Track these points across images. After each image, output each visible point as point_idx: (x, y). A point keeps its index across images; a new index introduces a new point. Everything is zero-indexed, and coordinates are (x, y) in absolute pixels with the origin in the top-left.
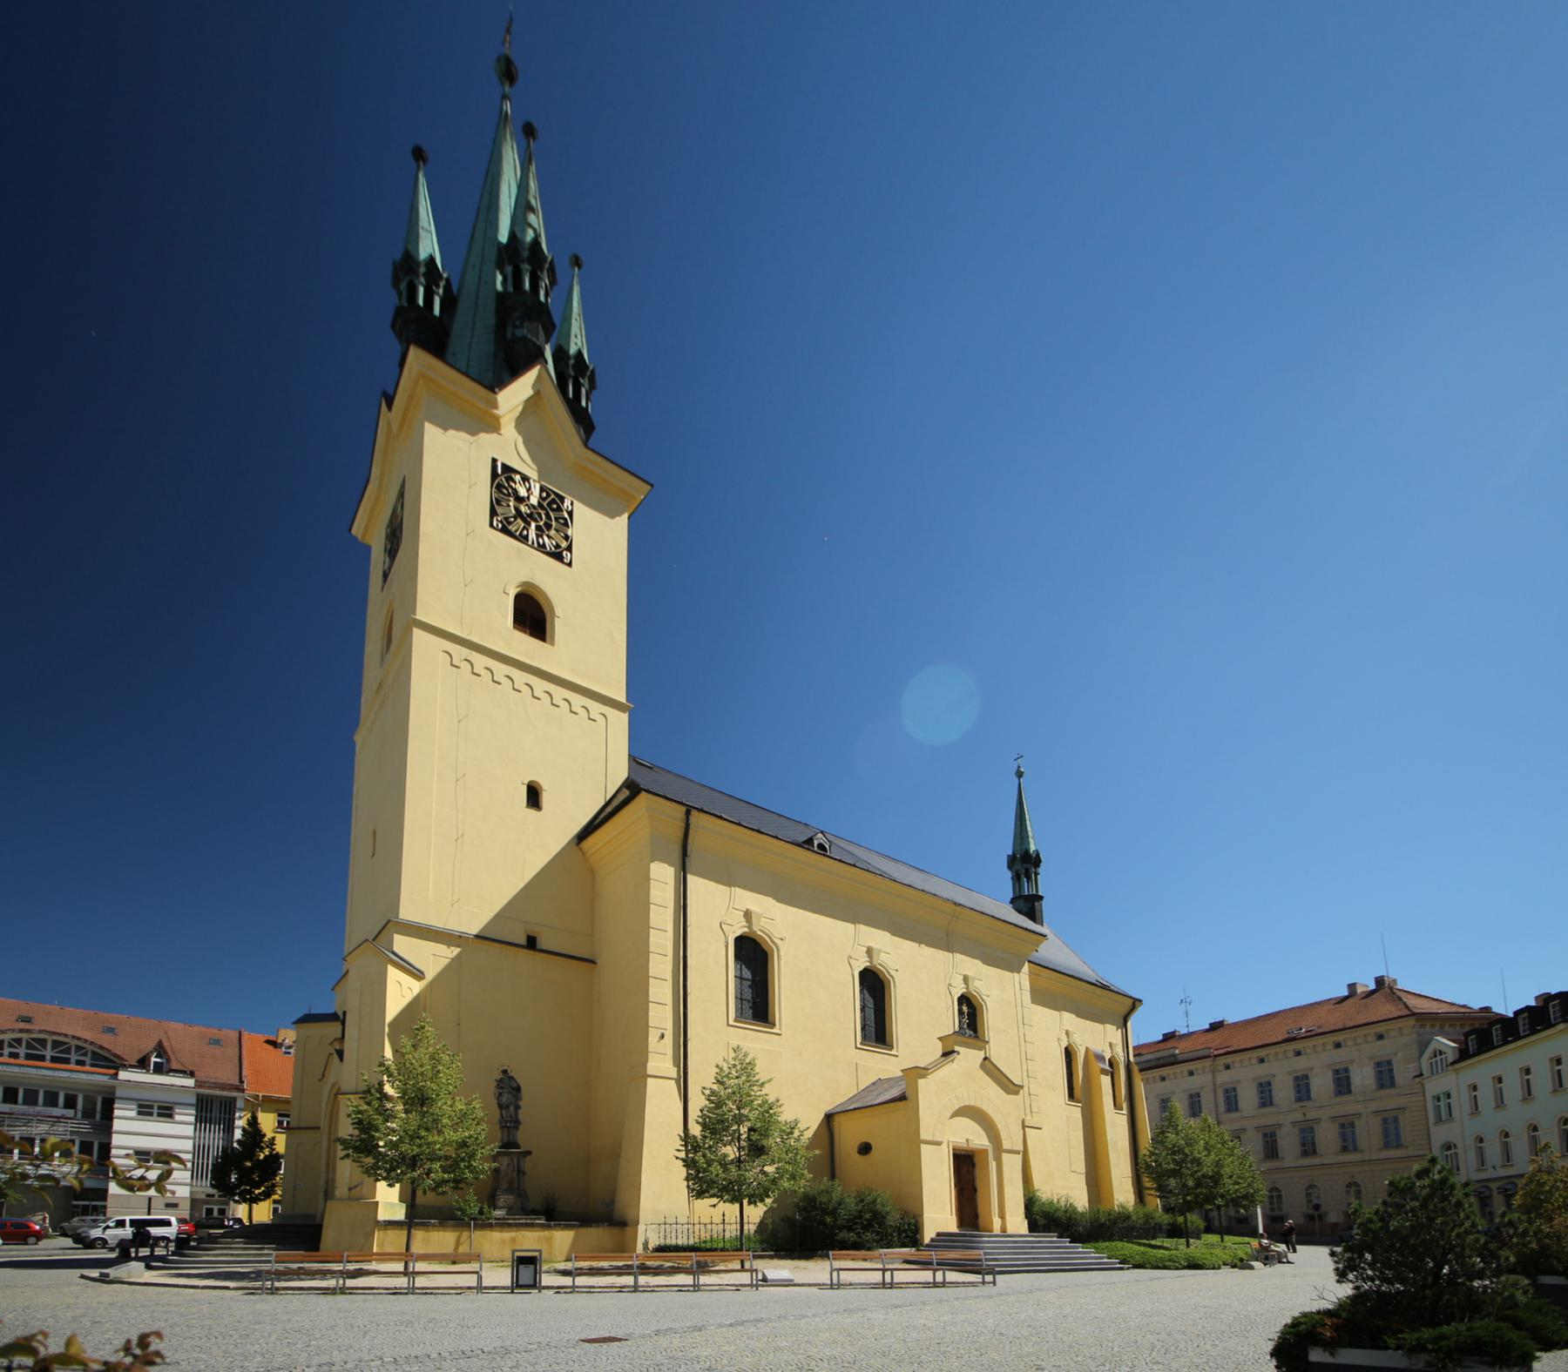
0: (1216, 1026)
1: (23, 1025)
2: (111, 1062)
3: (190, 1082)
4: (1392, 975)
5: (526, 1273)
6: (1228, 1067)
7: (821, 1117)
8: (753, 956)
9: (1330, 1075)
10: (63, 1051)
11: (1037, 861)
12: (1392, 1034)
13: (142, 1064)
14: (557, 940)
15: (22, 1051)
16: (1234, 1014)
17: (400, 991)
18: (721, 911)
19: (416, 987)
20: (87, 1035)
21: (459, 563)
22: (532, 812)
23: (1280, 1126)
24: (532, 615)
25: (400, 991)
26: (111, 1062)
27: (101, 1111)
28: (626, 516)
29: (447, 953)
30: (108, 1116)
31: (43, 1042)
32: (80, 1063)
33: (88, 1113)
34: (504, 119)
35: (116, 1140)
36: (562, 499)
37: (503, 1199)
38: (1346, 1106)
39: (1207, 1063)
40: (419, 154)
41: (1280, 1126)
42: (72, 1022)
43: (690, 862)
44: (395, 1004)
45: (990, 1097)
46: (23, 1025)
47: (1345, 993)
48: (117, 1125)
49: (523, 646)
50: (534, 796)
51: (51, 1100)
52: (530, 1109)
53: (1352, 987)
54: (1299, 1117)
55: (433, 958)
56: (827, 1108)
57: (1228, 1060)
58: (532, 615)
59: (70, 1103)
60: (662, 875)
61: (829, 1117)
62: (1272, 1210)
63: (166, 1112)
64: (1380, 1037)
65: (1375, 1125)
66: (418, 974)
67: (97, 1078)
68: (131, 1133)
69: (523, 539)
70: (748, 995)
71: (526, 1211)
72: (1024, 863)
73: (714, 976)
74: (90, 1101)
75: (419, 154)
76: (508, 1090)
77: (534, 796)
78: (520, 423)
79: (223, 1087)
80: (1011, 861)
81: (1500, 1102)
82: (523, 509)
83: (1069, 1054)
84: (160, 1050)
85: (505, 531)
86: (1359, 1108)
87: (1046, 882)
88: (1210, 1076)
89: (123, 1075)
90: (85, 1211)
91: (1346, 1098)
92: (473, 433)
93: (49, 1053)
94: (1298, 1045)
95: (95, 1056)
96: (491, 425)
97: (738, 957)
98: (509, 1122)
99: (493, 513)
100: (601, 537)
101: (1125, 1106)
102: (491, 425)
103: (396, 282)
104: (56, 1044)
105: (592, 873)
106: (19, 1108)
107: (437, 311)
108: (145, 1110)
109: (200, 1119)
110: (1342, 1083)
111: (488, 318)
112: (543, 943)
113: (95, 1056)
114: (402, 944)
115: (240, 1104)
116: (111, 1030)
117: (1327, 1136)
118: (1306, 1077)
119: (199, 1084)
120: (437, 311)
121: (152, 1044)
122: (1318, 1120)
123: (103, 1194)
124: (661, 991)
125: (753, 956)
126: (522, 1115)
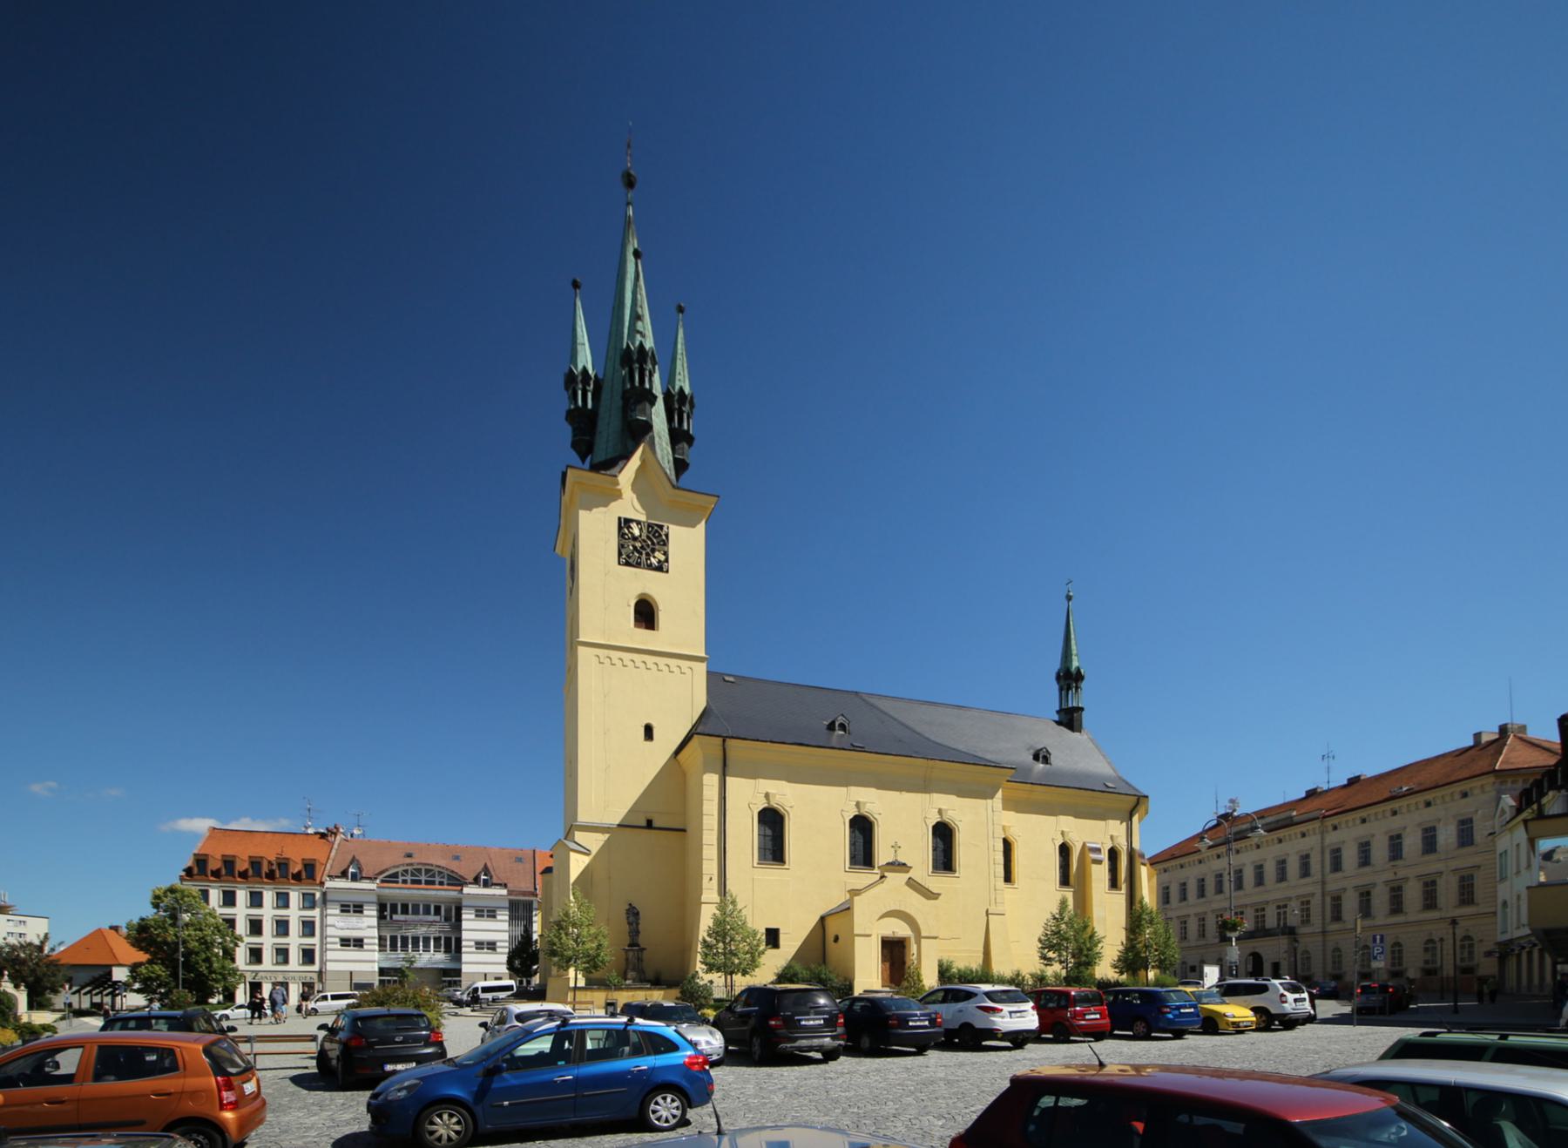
0: (1353, 781)
1: (408, 860)
2: (457, 881)
3: (504, 892)
4: (1518, 720)
5: (611, 1009)
6: (1335, 828)
7: (815, 919)
8: (772, 821)
9: (1419, 834)
11: (1079, 677)
12: (1476, 791)
13: (476, 881)
14: (661, 823)
15: (409, 878)
16: (1369, 770)
17: (577, 864)
18: (747, 796)
19: (586, 860)
20: (443, 863)
21: (604, 588)
22: (648, 743)
23: (1374, 885)
24: (646, 614)
25: (577, 864)
26: (457, 881)
27: (453, 915)
28: (701, 527)
29: (601, 838)
30: (459, 919)
31: (419, 871)
32: (441, 883)
33: (448, 950)
34: (628, 222)
35: (465, 935)
36: (661, 527)
37: (631, 974)
38: (1432, 865)
39: (1316, 824)
40: (576, 285)
41: (1374, 885)
43: (730, 768)
44: (574, 874)
45: (914, 904)
46: (408, 860)
47: (1471, 743)
48: (465, 925)
49: (643, 638)
50: (649, 732)
51: (427, 912)
52: (643, 925)
53: (1477, 736)
54: (1390, 876)
55: (595, 842)
56: (822, 913)
57: (1335, 820)
58: (646, 614)
59: (437, 911)
60: (711, 781)
61: (823, 919)
62: (1393, 964)
63: (492, 914)
64: (1465, 795)
65: (1454, 882)
66: (587, 852)
67: (449, 893)
68: (473, 930)
69: (638, 565)
70: (769, 845)
71: (641, 981)
72: (1069, 679)
73: (745, 835)
74: (448, 911)
75: (576, 285)
76: (633, 914)
77: (649, 732)
78: (635, 486)
79: (524, 894)
80: (1058, 678)
81: (1184, 898)
82: (638, 545)
83: (1065, 850)
84: (486, 870)
85: (628, 564)
86: (1440, 866)
87: (1085, 697)
88: (1319, 837)
89: (466, 890)
90: (450, 984)
91: (1432, 857)
92: (606, 505)
93: (423, 878)
94: (1395, 805)
96: (617, 495)
97: (760, 821)
98: (635, 932)
99: (620, 554)
100: (687, 544)
101: (1124, 886)
102: (617, 495)
103: (567, 389)
104: (427, 871)
105: (684, 774)
106: (410, 917)
107: (590, 405)
108: (480, 913)
109: (512, 918)
110: (1430, 842)
111: (618, 402)
112: (655, 824)
114: (579, 836)
115: (535, 905)
116: (457, 858)
117: (1413, 894)
118: (1399, 836)
119: (510, 893)
120: (590, 405)
121: (481, 866)
122: (1406, 879)
123: (458, 972)
124: (710, 853)
125: (772, 821)
126: (641, 927)
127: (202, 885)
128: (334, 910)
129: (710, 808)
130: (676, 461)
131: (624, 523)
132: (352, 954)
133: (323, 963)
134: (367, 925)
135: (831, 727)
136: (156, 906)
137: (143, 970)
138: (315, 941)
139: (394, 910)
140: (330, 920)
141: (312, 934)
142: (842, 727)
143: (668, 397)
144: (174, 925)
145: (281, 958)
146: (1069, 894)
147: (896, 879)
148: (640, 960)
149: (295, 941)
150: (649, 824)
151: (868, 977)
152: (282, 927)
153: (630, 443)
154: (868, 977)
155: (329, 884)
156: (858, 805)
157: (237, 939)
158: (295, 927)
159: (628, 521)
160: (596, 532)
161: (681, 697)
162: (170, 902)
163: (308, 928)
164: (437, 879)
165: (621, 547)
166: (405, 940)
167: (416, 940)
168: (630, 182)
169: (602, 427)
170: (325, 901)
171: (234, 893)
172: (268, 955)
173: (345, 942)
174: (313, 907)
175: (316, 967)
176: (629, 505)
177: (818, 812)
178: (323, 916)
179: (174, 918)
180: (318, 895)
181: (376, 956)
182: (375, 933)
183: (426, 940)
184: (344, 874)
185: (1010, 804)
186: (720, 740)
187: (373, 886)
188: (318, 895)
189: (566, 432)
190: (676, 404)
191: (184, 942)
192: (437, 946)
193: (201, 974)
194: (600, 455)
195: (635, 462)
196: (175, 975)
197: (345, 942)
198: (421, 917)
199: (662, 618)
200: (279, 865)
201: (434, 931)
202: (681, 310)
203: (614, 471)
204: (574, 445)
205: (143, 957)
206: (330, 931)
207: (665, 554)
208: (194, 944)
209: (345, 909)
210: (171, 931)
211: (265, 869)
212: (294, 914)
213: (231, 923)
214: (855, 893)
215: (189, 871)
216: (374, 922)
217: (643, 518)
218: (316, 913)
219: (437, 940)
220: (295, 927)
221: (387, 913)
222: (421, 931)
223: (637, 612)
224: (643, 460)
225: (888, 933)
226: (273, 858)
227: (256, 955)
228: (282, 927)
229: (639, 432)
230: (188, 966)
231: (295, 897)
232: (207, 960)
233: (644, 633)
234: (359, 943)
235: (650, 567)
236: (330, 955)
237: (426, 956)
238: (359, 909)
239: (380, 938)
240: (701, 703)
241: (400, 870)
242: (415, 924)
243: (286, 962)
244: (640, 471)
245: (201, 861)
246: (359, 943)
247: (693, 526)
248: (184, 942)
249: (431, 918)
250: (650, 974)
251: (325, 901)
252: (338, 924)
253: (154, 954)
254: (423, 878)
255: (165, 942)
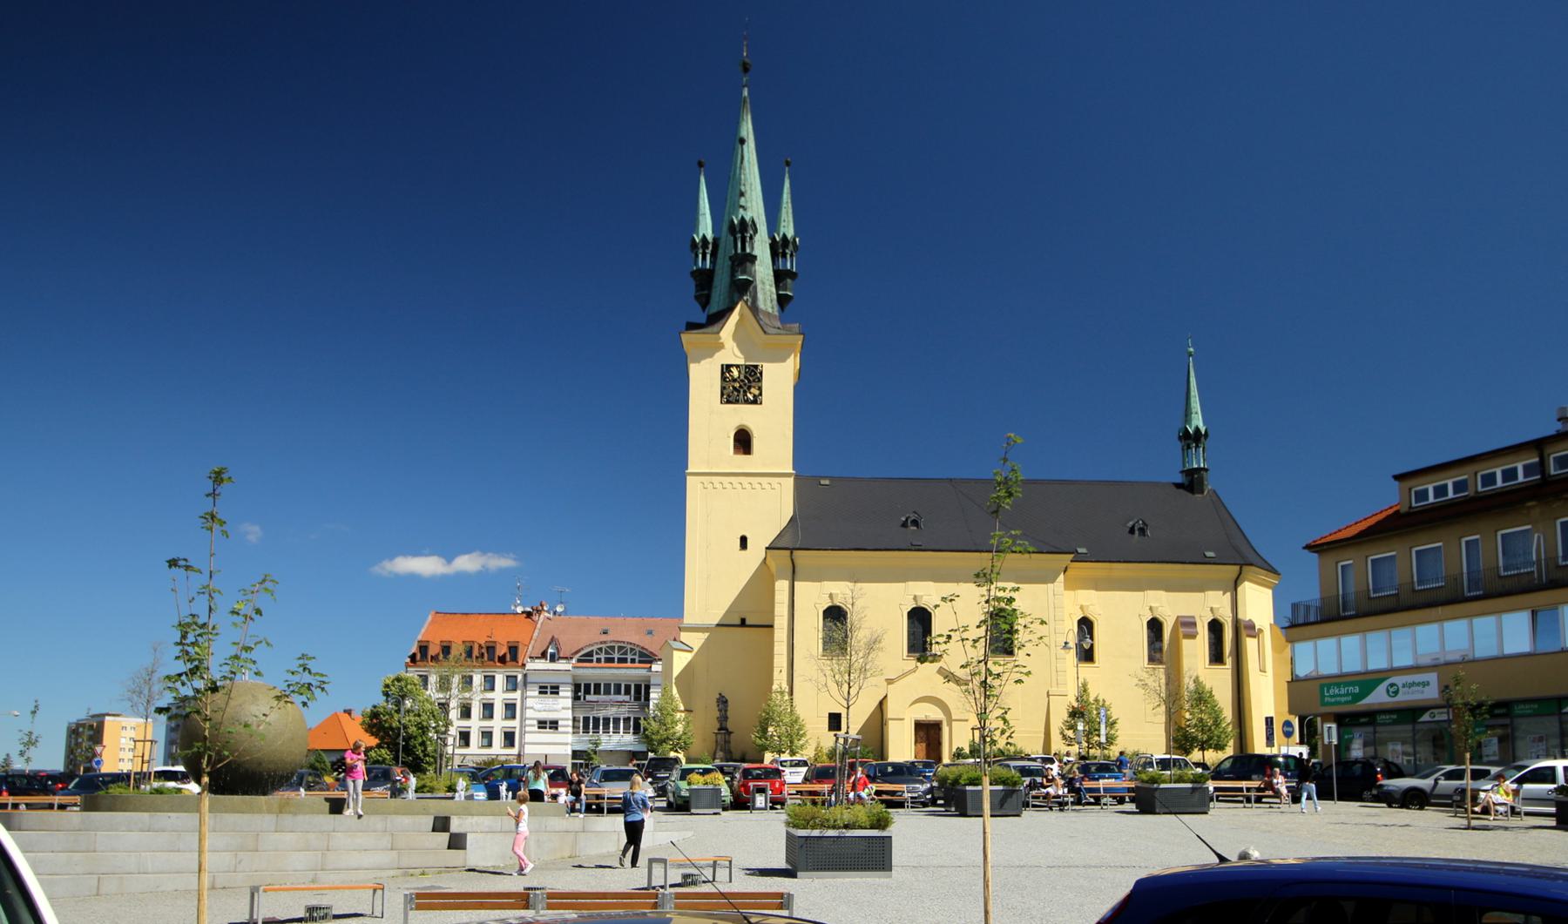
1: (604, 638)
10: (618, 654)
14: (748, 622)
15: (603, 656)
17: (680, 661)
18: (813, 596)
19: (688, 657)
21: (709, 419)
24: (743, 441)
29: (703, 636)
31: (612, 648)
32: (633, 661)
42: (628, 631)
46: (604, 638)
50: (744, 542)
51: (618, 692)
55: (696, 640)
58: (743, 441)
59: (628, 692)
66: (690, 650)
69: (737, 402)
73: (811, 627)
74: (638, 687)
76: (723, 702)
77: (744, 542)
78: (736, 337)
83: (1155, 626)
85: (728, 402)
93: (616, 656)
95: (642, 655)
96: (721, 346)
98: (723, 718)
100: (780, 378)
101: (1229, 661)
102: (721, 346)
104: (620, 648)
106: (602, 697)
113: (642, 655)
114: (684, 636)
116: (650, 633)
127: (422, 670)
128: (533, 692)
129: (781, 610)
130: (779, 296)
131: (726, 368)
132: (548, 736)
133: (522, 746)
134: (561, 707)
135: (904, 525)
136: (386, 694)
137: (372, 754)
138: (515, 723)
139: (587, 691)
140: (529, 702)
141: (514, 717)
142: (915, 523)
143: (774, 247)
144: (398, 711)
145: (486, 741)
146: (1161, 670)
147: (929, 668)
148: (727, 742)
149: (498, 724)
150: (743, 623)
151: (902, 748)
152: (488, 709)
153: (736, 295)
154: (902, 748)
155: (530, 666)
156: (915, 598)
157: (448, 724)
158: (499, 710)
159: (729, 366)
160: (704, 379)
161: (773, 506)
162: (397, 692)
163: (510, 709)
164: (629, 657)
165: (723, 388)
166: (596, 720)
167: (606, 720)
168: (746, 69)
169: (714, 289)
170: (525, 683)
171: (471, 678)
172: (475, 738)
173: (542, 724)
174: (515, 690)
175: (515, 751)
176: (731, 354)
177: (881, 605)
178: (524, 698)
179: (398, 703)
180: (520, 677)
181: (570, 738)
182: (569, 714)
183: (617, 721)
184: (544, 655)
185: (1069, 586)
186: (787, 553)
187: (569, 667)
188: (520, 677)
189: (691, 286)
190: (778, 249)
191: (405, 727)
192: (626, 729)
193: (418, 757)
194: (714, 307)
195: (734, 317)
196: (396, 759)
197: (542, 724)
198: (613, 697)
199: (756, 444)
200: (488, 648)
201: (623, 712)
202: (788, 164)
203: (715, 328)
204: (697, 298)
205: (374, 741)
206: (529, 713)
207: (760, 389)
208: (412, 730)
209: (543, 690)
210: (396, 717)
211: (476, 653)
212: (499, 697)
213: (444, 706)
214: (890, 681)
215: (413, 658)
216: (569, 703)
217: (741, 362)
218: (517, 695)
219: (627, 720)
220: (499, 710)
221: (581, 694)
222: (611, 712)
223: (736, 440)
224: (741, 315)
225: (921, 717)
226: (482, 642)
227: (465, 737)
228: (488, 709)
229: (742, 288)
230: (408, 750)
231: (500, 680)
232: (423, 744)
233: (742, 458)
234: (554, 725)
235: (747, 402)
236: (528, 738)
237: (615, 738)
238: (555, 690)
239: (574, 719)
240: (788, 512)
241: (595, 648)
242: (605, 705)
243: (490, 745)
244: (738, 324)
245: (423, 648)
246: (554, 725)
247: (783, 360)
248: (405, 727)
249: (622, 697)
250: (737, 755)
251: (525, 683)
252: (537, 706)
253: (382, 739)
254: (616, 656)
255: (391, 728)
